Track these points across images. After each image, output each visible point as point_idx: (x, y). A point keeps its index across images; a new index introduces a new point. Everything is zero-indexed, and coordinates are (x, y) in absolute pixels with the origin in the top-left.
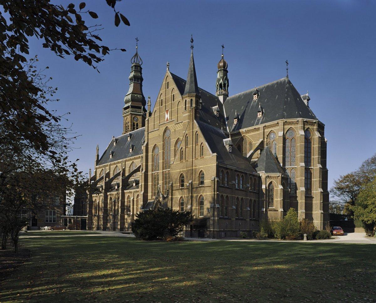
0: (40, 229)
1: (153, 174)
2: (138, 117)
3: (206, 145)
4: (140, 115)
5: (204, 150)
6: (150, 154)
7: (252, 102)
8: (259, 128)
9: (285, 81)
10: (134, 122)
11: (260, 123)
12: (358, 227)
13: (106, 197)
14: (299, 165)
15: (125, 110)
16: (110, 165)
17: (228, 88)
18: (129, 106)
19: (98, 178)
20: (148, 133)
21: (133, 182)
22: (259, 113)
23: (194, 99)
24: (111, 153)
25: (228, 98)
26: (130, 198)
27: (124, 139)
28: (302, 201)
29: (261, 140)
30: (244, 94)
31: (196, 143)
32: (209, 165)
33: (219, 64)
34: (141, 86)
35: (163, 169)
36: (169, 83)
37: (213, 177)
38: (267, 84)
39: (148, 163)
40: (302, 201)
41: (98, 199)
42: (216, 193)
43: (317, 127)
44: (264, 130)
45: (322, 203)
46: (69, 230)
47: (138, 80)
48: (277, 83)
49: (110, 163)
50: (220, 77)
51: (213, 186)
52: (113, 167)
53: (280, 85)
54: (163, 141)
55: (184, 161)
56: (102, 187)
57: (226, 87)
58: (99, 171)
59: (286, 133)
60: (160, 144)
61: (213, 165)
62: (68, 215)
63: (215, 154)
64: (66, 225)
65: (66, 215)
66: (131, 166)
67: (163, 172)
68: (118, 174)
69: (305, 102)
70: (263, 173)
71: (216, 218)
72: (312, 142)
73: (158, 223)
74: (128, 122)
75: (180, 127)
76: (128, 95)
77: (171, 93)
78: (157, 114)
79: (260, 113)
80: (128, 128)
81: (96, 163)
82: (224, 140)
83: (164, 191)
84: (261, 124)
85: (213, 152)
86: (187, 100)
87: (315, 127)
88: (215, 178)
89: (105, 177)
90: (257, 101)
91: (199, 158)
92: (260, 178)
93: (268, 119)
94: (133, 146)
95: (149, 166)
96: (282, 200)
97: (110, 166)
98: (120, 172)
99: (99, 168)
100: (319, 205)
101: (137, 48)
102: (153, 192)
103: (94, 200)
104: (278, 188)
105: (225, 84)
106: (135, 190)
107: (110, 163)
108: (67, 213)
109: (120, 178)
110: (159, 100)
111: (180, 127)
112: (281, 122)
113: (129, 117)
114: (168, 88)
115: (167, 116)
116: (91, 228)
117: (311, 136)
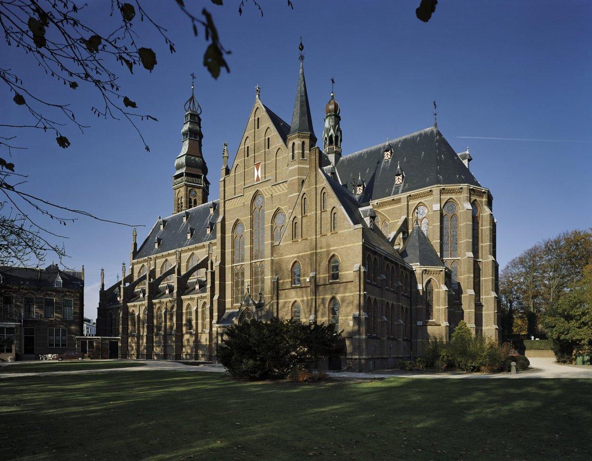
0: (38, 359)
1: (234, 267)
2: (197, 190)
4: (199, 188)
5: (338, 219)
6: (228, 235)
7: (382, 162)
8: (400, 199)
9: (432, 132)
10: (191, 197)
11: (400, 191)
12: (531, 348)
13: (151, 306)
14: (465, 255)
15: (175, 179)
16: (155, 259)
17: (340, 143)
18: (183, 173)
19: (136, 278)
20: (225, 202)
21: (194, 284)
22: (397, 178)
23: (307, 141)
24: (156, 241)
25: (341, 158)
26: (190, 308)
27: (177, 221)
28: (470, 310)
29: (403, 218)
30: (367, 152)
31: (322, 209)
32: (348, 245)
33: (327, 107)
34: (200, 145)
35: (252, 259)
36: (260, 120)
37: (358, 265)
38: (404, 137)
39: (225, 250)
40: (470, 310)
41: (138, 308)
42: (362, 293)
43: (487, 200)
44: (408, 202)
45: (496, 314)
46: (89, 360)
47: (195, 135)
48: (420, 135)
49: (155, 256)
50: (329, 127)
51: (357, 280)
52: (160, 262)
53: (427, 138)
54: (251, 214)
55: (300, 240)
56: (144, 292)
57: (339, 142)
58: (137, 268)
59: (444, 206)
60: (245, 219)
61: (357, 245)
62: (91, 335)
64: (84, 351)
65: (83, 335)
66: (191, 260)
67: (251, 264)
68: (172, 271)
69: (465, 162)
70: (418, 265)
71: (364, 337)
72: (480, 222)
73: (260, 346)
74: (182, 197)
76: (181, 157)
77: (264, 135)
78: (240, 171)
79: (400, 177)
80: (182, 206)
81: (132, 255)
82: (360, 209)
83: (253, 294)
84: (402, 192)
86: (296, 143)
87: (484, 199)
89: (149, 275)
90: (390, 161)
91: (329, 234)
92: (412, 273)
93: (413, 186)
94: (192, 231)
95: (226, 254)
96: (447, 308)
98: (175, 267)
99: (138, 263)
100: (493, 316)
101: (193, 88)
102: (234, 296)
103: (131, 310)
104: (441, 290)
105: (337, 137)
106: (199, 295)
107: (155, 256)
108: (85, 333)
109: (175, 276)
110: (242, 147)
111: (282, 189)
112: (436, 189)
113: (183, 190)
114: (258, 128)
115: (258, 173)
116: (125, 355)
117: (478, 213)
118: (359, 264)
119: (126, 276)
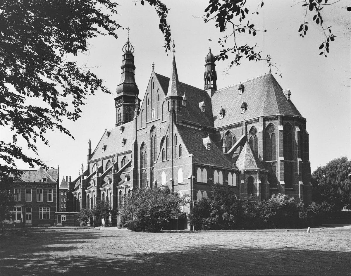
3: (184, 146)
44: (246, 125)
55: (166, 161)
63: (191, 155)
66: (124, 161)
75: (165, 126)
85: (190, 153)
88: (191, 177)
97: (102, 161)
113: (121, 108)
118: (191, 175)
119: (84, 171)
